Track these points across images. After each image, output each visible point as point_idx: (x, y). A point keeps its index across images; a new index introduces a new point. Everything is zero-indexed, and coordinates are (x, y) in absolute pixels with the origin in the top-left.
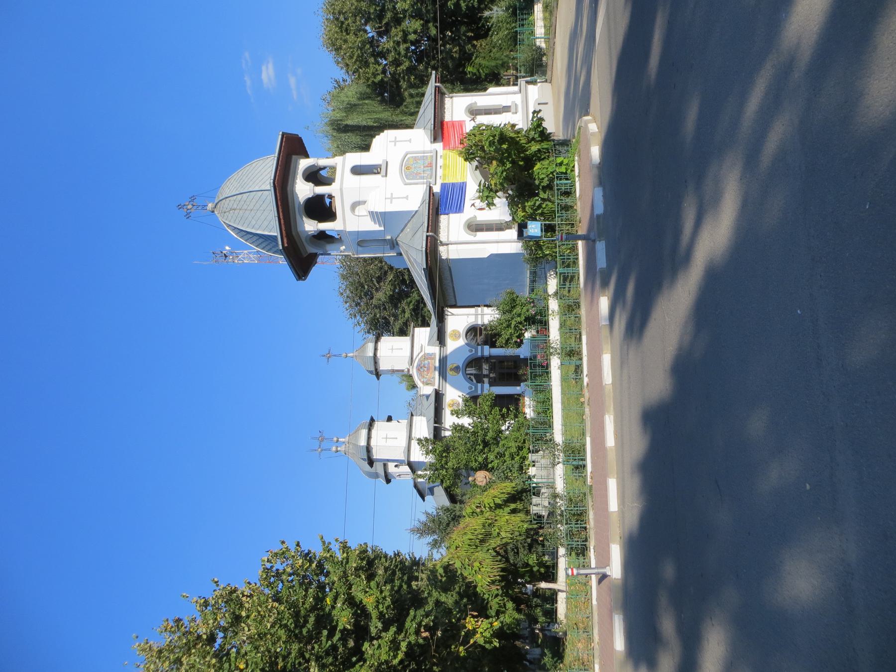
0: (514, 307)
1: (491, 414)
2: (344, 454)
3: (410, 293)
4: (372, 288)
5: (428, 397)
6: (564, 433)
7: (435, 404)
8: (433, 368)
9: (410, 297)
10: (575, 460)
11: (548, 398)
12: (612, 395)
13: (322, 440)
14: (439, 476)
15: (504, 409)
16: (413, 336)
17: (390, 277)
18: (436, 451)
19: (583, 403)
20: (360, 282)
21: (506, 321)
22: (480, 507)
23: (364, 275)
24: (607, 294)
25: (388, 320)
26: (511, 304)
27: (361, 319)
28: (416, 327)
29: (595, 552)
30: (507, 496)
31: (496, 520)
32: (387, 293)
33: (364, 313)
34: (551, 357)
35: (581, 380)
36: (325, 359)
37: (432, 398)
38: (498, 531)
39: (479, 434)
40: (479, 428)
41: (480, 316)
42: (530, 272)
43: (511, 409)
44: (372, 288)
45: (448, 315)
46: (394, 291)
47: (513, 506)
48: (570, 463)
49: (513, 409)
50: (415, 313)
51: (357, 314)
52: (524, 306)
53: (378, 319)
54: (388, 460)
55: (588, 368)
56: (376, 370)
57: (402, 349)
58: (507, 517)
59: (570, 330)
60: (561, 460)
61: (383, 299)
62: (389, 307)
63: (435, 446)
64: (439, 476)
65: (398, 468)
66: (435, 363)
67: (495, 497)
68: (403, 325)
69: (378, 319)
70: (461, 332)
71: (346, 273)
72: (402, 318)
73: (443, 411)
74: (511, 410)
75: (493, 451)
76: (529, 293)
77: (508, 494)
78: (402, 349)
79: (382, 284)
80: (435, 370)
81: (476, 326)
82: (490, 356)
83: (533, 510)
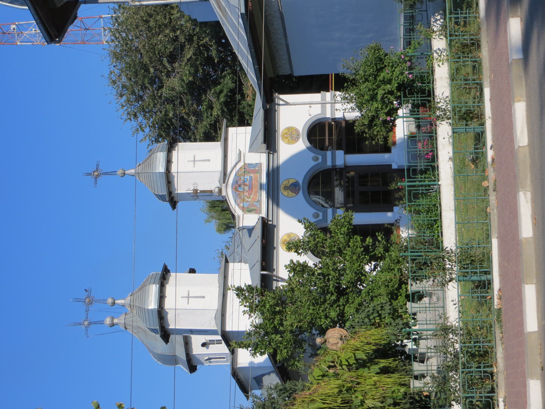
0: (380, 70)
1: (349, 246)
2: (123, 328)
3: (221, 78)
4: (161, 72)
5: (250, 230)
6: (459, 232)
7: (262, 241)
8: (259, 185)
9: (220, 84)
10: (476, 273)
11: (435, 205)
12: (528, 161)
13: (90, 303)
14: (270, 344)
15: (368, 239)
16: (226, 139)
17: (189, 53)
18: (264, 306)
19: (486, 189)
20: (142, 63)
21: (369, 90)
22: (335, 366)
23: (147, 52)
24: (519, 13)
25: (187, 121)
26: (376, 64)
27: (145, 121)
28: (230, 126)
29: (505, 405)
30: (374, 348)
31: (358, 383)
32: (185, 78)
33: (149, 112)
34: (438, 123)
35: (484, 154)
36: (91, 179)
37: (258, 233)
38: (362, 398)
39: (330, 277)
40: (331, 268)
41: (328, 106)
42: (405, 16)
43: (379, 238)
44: (161, 72)
45: (279, 105)
46: (195, 75)
47: (383, 363)
48: (468, 278)
49: (382, 238)
50: (228, 109)
51: (138, 114)
52: (396, 68)
53: (170, 120)
54: (192, 332)
55: (494, 136)
56: (170, 193)
57: (209, 160)
58: (375, 379)
59: (466, 80)
60: (454, 276)
61: (178, 88)
62: (188, 101)
63: (264, 298)
64: (270, 344)
65: (208, 348)
66: (261, 179)
67: (356, 350)
68: (211, 129)
69: (170, 120)
70: (301, 131)
71: (121, 51)
72: (207, 117)
73: (275, 251)
74: (379, 241)
75: (353, 302)
76: (404, 48)
77: (376, 344)
78: (209, 160)
79: (176, 65)
80: (261, 189)
81: (324, 120)
82: (345, 166)
83: (412, 308)
